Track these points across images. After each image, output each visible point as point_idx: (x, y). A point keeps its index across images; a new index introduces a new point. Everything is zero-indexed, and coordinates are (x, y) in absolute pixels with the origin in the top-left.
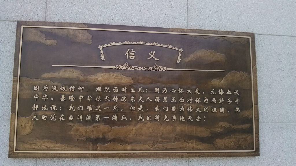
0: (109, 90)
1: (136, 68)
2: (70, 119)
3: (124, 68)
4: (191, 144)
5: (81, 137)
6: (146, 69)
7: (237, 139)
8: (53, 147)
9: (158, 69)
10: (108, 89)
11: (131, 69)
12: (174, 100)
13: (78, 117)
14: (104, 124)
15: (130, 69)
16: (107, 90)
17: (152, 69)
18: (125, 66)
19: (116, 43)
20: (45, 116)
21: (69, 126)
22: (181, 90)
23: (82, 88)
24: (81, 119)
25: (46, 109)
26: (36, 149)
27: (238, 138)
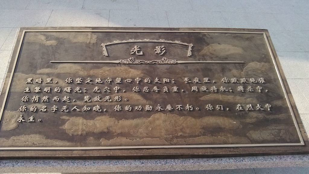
0: (47, 100)
1: (143, 62)
4: (220, 137)
6: (154, 62)
7: (277, 131)
8: (41, 143)
10: (46, 99)
14: (110, 117)
16: (45, 99)
18: (130, 60)
20: (34, 108)
21: (64, 119)
22: (206, 80)
25: (101, 82)
26: (55, 27)
27: (277, 129)
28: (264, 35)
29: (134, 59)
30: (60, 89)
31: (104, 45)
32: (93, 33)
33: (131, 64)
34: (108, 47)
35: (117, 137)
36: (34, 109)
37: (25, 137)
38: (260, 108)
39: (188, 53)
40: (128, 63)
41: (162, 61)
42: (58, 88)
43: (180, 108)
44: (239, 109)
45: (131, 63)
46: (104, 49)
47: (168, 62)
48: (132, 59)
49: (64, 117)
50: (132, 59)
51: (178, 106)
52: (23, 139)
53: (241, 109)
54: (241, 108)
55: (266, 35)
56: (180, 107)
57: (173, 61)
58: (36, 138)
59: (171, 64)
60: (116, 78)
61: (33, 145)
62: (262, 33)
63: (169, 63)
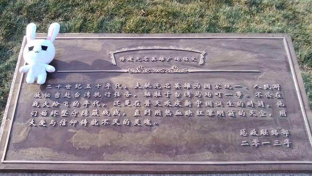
1: (152, 71)
2: (76, 96)
3: (137, 71)
5: (83, 145)
6: (164, 71)
9: (178, 71)
11: (146, 72)
12: (178, 103)
13: (85, 94)
15: (144, 72)
17: (170, 71)
18: (139, 69)
19: (129, 49)
23: (74, 122)
24: (88, 96)
28: (284, 40)
29: (143, 68)
30: (78, 103)
31: (113, 54)
32: (99, 40)
33: (139, 73)
34: (116, 55)
35: (120, 152)
36: (127, 123)
37: (33, 150)
38: (157, 105)
39: (200, 61)
40: (136, 72)
41: (172, 70)
42: (77, 103)
43: (106, 123)
44: (278, 97)
45: (140, 72)
46: (112, 57)
47: (178, 71)
48: (141, 68)
49: (71, 130)
50: (141, 68)
51: (104, 120)
52: (31, 152)
53: (279, 97)
54: (279, 96)
55: (286, 40)
56: (106, 121)
57: (183, 70)
58: (40, 151)
59: (181, 72)
60: (217, 112)
61: (41, 159)
62: (282, 38)
63: (179, 72)
